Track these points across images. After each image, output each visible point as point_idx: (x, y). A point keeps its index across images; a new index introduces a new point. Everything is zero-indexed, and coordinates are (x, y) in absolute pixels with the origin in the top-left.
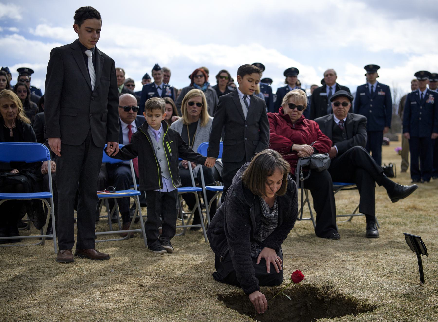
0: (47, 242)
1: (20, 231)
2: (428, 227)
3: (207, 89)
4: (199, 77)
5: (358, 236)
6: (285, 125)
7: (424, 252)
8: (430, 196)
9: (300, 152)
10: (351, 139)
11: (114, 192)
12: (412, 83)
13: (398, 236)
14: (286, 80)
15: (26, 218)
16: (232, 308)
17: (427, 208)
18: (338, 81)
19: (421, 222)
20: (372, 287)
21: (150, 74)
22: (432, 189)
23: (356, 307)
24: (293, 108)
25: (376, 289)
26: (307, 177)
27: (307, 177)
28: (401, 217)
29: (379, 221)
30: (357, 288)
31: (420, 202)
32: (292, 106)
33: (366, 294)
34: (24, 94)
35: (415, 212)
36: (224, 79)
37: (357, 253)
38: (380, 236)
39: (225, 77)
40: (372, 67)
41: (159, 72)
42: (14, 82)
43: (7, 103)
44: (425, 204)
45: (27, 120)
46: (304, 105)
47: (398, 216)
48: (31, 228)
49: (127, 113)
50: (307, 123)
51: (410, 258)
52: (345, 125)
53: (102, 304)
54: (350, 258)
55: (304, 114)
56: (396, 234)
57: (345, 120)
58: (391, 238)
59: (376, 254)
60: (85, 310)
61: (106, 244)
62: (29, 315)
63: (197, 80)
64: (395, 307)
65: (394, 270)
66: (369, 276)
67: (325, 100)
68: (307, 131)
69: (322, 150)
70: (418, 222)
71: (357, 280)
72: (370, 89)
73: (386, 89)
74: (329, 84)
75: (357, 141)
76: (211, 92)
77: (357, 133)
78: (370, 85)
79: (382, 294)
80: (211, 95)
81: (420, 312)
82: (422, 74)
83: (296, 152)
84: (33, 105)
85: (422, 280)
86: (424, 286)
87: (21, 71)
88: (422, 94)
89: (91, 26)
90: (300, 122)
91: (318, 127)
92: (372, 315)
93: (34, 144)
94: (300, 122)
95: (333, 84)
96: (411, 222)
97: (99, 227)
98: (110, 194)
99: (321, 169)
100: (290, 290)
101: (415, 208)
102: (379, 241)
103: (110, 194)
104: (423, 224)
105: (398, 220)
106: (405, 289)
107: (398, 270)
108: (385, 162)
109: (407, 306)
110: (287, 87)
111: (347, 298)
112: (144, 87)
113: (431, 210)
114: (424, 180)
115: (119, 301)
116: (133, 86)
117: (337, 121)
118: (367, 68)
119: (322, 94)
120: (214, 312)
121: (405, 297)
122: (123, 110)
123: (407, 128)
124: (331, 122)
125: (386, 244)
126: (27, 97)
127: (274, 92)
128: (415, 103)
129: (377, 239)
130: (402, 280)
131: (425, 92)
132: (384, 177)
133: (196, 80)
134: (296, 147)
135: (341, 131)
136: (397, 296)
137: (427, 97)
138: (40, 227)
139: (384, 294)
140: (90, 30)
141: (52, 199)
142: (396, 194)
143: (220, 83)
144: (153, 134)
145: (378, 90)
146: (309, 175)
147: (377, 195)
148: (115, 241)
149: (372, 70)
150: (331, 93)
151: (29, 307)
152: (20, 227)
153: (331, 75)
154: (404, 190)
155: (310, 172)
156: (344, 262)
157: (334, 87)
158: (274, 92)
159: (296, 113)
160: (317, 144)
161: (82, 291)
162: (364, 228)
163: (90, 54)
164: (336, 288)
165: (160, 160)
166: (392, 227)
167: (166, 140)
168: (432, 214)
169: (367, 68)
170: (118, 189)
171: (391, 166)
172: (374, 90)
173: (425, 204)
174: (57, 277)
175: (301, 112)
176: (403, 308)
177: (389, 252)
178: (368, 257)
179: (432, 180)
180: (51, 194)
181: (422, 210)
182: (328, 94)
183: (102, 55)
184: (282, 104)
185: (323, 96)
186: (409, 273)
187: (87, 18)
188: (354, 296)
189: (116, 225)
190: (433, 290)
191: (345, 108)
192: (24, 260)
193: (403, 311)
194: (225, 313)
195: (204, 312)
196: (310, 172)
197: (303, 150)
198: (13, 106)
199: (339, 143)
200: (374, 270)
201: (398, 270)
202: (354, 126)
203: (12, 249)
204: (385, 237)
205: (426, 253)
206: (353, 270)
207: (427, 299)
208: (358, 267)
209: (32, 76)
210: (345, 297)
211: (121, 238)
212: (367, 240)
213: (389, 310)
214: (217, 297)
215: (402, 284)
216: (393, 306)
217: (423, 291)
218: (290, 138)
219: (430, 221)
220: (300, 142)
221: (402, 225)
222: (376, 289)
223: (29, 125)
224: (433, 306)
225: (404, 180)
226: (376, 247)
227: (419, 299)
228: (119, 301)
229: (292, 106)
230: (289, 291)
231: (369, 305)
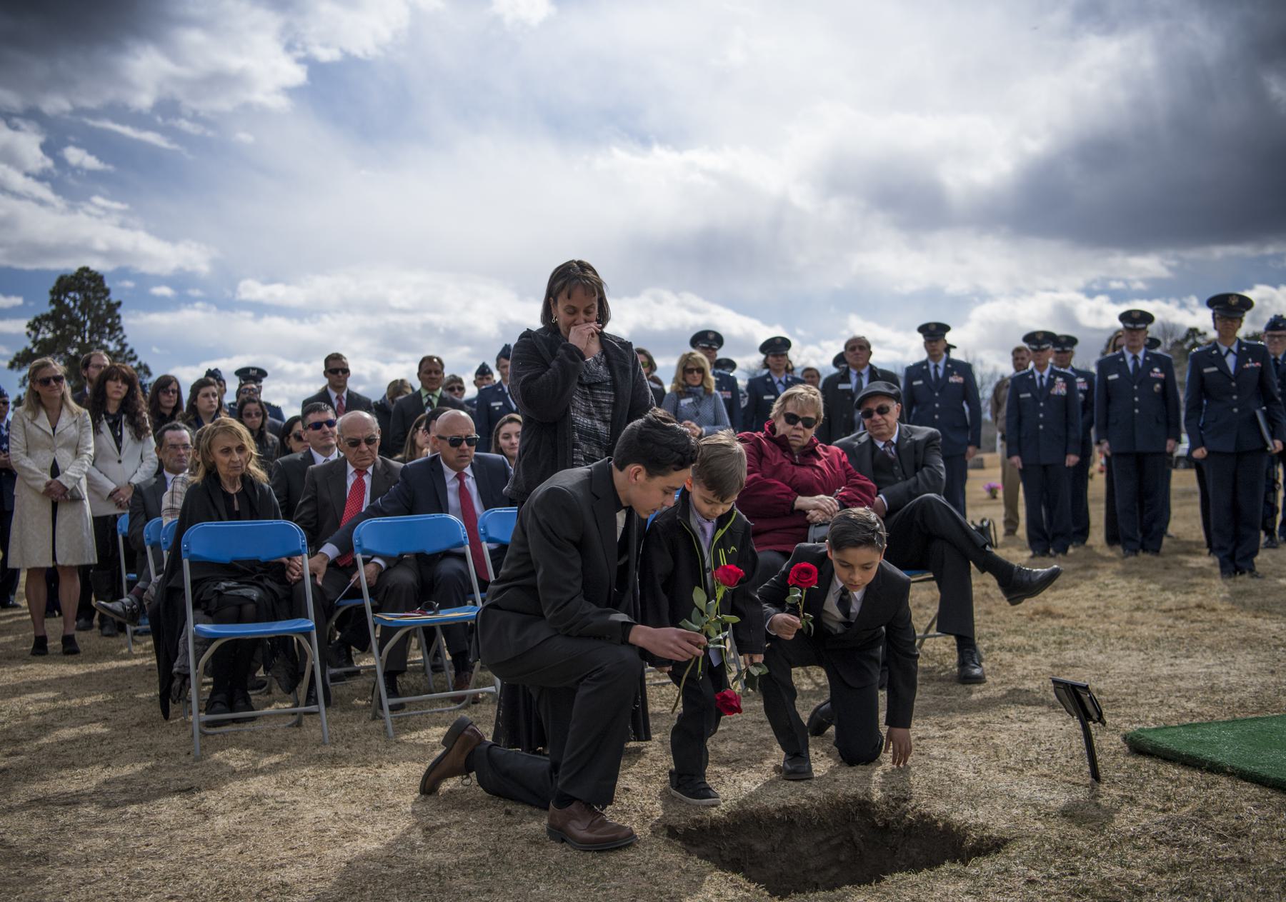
0: (306, 719)
1: (253, 698)
2: (1082, 653)
5: (941, 680)
6: (777, 457)
7: (1095, 717)
8: (1075, 586)
9: (812, 512)
10: (913, 479)
11: (436, 613)
12: (1013, 353)
13: (1024, 677)
14: (765, 361)
15: (260, 673)
16: (700, 857)
17: (1074, 611)
18: (872, 360)
19: (1067, 643)
20: (991, 795)
21: (492, 365)
22: (1075, 570)
23: (961, 844)
24: (794, 423)
25: (1000, 801)
28: (1023, 633)
29: (982, 645)
30: (958, 799)
31: (1056, 599)
32: (791, 419)
33: (980, 812)
35: (1050, 621)
37: (947, 721)
38: (988, 677)
40: (933, 328)
42: (230, 398)
43: (229, 444)
44: (1067, 603)
45: (261, 475)
46: (818, 418)
47: (1016, 631)
48: (274, 690)
49: (455, 449)
50: (822, 453)
51: (1058, 727)
52: (897, 450)
53: (429, 856)
54: (935, 732)
55: (818, 434)
56: (1019, 673)
57: (894, 439)
58: (1009, 682)
59: (986, 719)
60: (395, 871)
61: (423, 719)
62: (285, 885)
64: (1048, 840)
65: (1032, 755)
66: (979, 772)
68: (826, 468)
70: (1060, 643)
71: (957, 781)
72: (932, 371)
73: (965, 369)
74: (855, 367)
75: (925, 480)
77: (924, 466)
78: (932, 364)
79: (1014, 811)
81: (1102, 849)
82: (1039, 337)
83: (803, 512)
85: (1095, 775)
86: (1102, 788)
87: (244, 374)
88: (1042, 377)
90: (809, 452)
91: (845, 459)
92: (1001, 861)
93: (275, 522)
94: (809, 452)
95: (863, 366)
96: (1046, 644)
97: (408, 683)
98: (428, 618)
100: (818, 809)
101: (1048, 613)
102: (988, 689)
103: (428, 618)
104: (1070, 646)
105: (1019, 640)
106: (1060, 799)
107: (1038, 754)
108: (973, 517)
109: (1073, 837)
110: (768, 375)
111: (941, 824)
112: (481, 392)
113: (1083, 616)
114: (1057, 552)
115: (463, 847)
116: (462, 389)
118: (924, 329)
119: (841, 386)
120: (665, 868)
121: (1064, 816)
122: (447, 444)
123: (1015, 445)
124: (868, 447)
125: (1004, 697)
126: (262, 425)
127: (742, 383)
128: (1029, 395)
129: (982, 687)
130: (1051, 777)
131: (1046, 374)
132: (974, 549)
134: (802, 501)
135: (891, 462)
136: (1047, 814)
137: (1051, 383)
138: (291, 688)
139: (1019, 811)
141: (314, 633)
142: (1017, 586)
145: (948, 372)
147: (976, 591)
148: (442, 712)
149: (934, 333)
150: (860, 385)
151: (282, 866)
152: (253, 689)
153: (861, 348)
154: (1034, 579)
156: (923, 742)
157: (865, 371)
158: (742, 383)
159: (801, 433)
160: (845, 494)
161: (384, 827)
162: (952, 662)
164: (913, 803)
166: (1007, 657)
168: (1084, 624)
169: (924, 329)
170: (446, 605)
171: (985, 524)
172: (940, 373)
173: (1067, 603)
174: (333, 796)
175: (811, 433)
176: (1066, 842)
177: (1012, 712)
178: (970, 727)
179: (1071, 551)
180: (312, 624)
181: (1063, 616)
182: (852, 386)
184: (772, 415)
185: (844, 390)
186: (1063, 760)
188: (956, 817)
189: (440, 677)
190: (1122, 797)
191: (887, 417)
192: (266, 761)
193: (1064, 849)
194: (688, 871)
195: (643, 868)
197: (816, 508)
198: (241, 449)
199: (888, 489)
200: (988, 758)
201: (1038, 754)
202: (916, 452)
203: (240, 737)
204: (998, 680)
205: (1100, 718)
206: (945, 759)
207: (1111, 819)
208: (953, 751)
209: (265, 382)
210: (936, 821)
211: (453, 707)
212: (960, 689)
213: (1036, 848)
214: (666, 832)
215: (1054, 787)
216: (1044, 839)
217: (1100, 801)
218: (789, 484)
219: (1085, 640)
220: (811, 492)
221: (1028, 652)
222: (1000, 801)
223: (267, 486)
224: (1129, 834)
225: (1018, 555)
226: (987, 704)
227: (1095, 819)
228: (463, 847)
229: (791, 419)
230: (814, 811)
231: (990, 837)
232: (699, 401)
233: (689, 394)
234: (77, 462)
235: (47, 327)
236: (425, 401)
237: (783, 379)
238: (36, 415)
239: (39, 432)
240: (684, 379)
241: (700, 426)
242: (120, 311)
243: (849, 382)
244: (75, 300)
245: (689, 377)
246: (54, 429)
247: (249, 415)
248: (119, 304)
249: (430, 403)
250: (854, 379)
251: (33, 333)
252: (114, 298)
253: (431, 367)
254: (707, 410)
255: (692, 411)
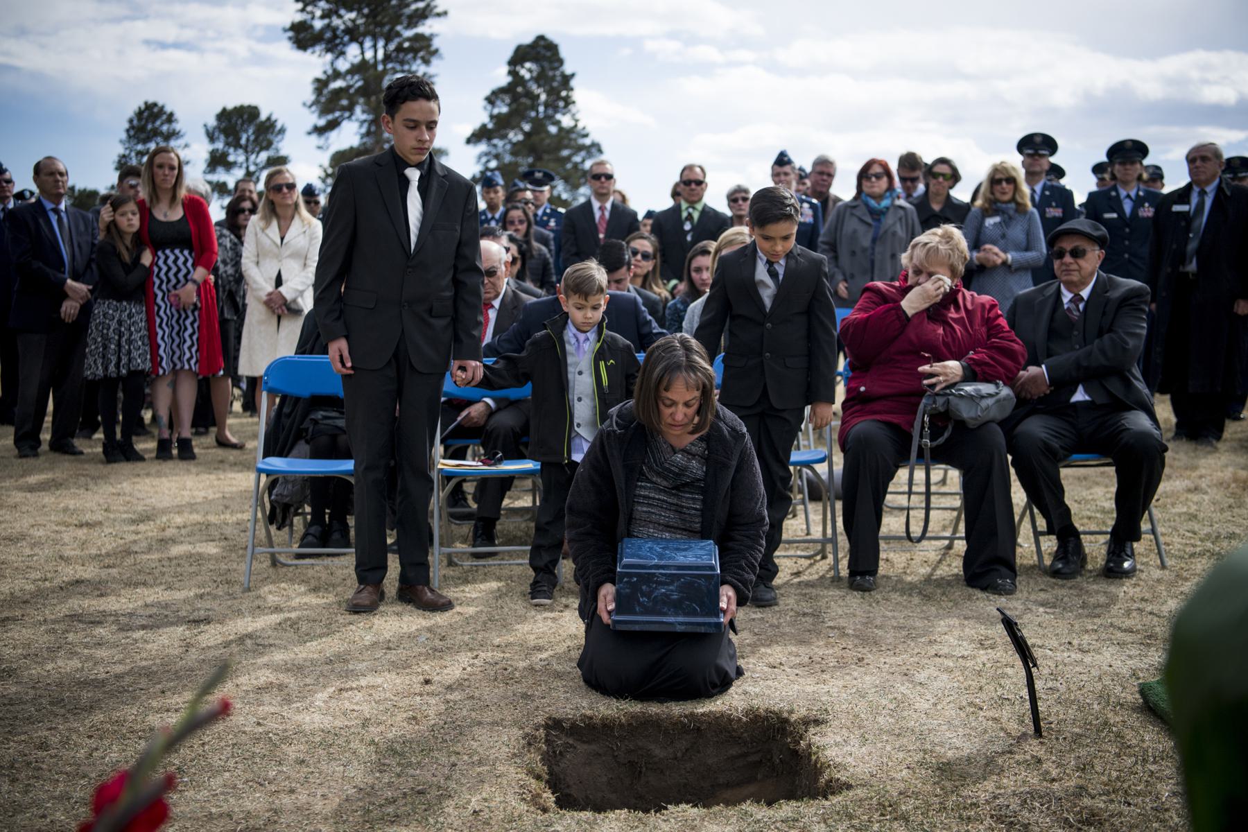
3: (892, 204)
4: (874, 179)
26: (941, 440)
27: (941, 440)
34: (520, 227)
36: (941, 179)
39: (943, 175)
41: (787, 169)
63: (868, 184)
67: (1183, 224)
69: (987, 369)
76: (901, 212)
80: (900, 219)
84: (540, 250)
89: (415, 117)
99: (973, 422)
117: (1067, 296)
119: (1177, 208)
124: (1051, 301)
133: (865, 184)
140: (412, 124)
143: (932, 188)
144: (573, 341)
146: (946, 435)
155: (950, 428)
163: (414, 175)
165: (580, 399)
167: (599, 356)
183: (444, 177)
185: (1179, 213)
187: (405, 100)
191: (1082, 262)
196: (950, 428)
232: (1007, 221)
233: (996, 212)
234: (303, 274)
235: (503, 101)
236: (684, 214)
237: (1133, 194)
238: (268, 224)
239: (269, 242)
240: (992, 193)
241: (1005, 251)
242: (573, 83)
243: (1188, 203)
244: (530, 71)
245: (998, 188)
246: (282, 239)
247: (512, 223)
248: (573, 75)
249: (690, 217)
250: (1194, 199)
251: (489, 107)
252: (568, 71)
253: (692, 177)
254: (1017, 232)
255: (999, 232)
